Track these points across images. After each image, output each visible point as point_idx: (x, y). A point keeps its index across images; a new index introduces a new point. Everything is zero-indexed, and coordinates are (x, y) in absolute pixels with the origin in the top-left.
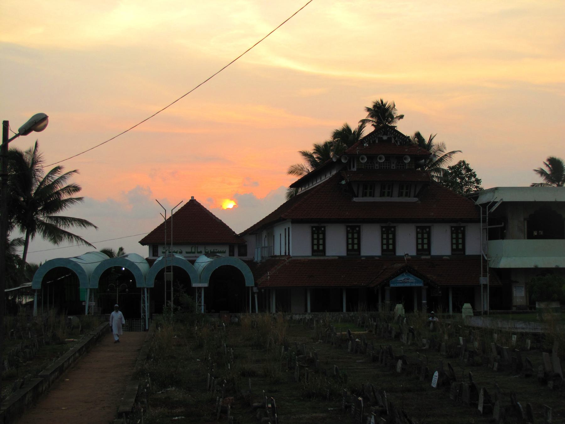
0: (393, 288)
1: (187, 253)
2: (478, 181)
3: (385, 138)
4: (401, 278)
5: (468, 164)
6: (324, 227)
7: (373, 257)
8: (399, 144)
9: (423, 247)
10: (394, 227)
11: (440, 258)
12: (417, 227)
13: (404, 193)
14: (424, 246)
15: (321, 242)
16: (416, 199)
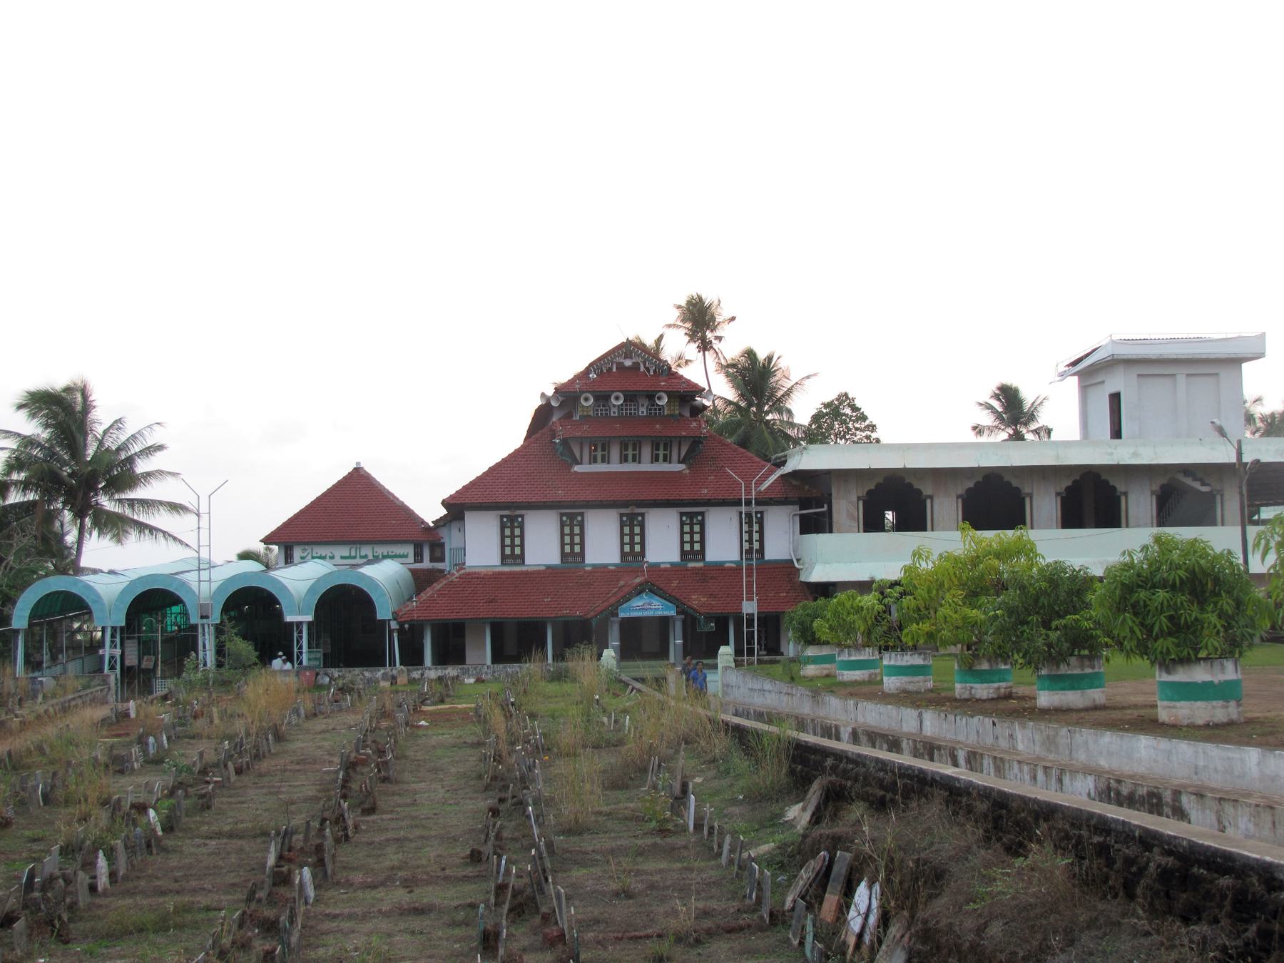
0: (623, 619)
1: (342, 558)
2: (872, 427)
3: (628, 363)
4: (637, 602)
6: (522, 516)
7: (605, 566)
9: (692, 547)
10: (643, 515)
11: (601, 569)
12: (682, 514)
13: (630, 458)
14: (693, 549)
15: (577, 539)
16: (682, 467)
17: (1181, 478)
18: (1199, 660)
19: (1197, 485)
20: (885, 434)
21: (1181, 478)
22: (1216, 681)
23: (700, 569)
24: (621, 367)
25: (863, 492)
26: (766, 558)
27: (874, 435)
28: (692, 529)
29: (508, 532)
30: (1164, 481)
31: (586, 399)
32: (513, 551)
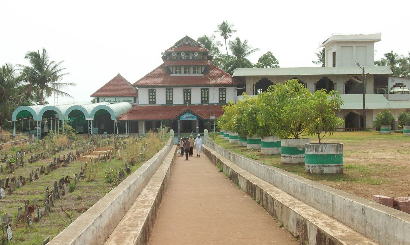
3: (187, 43)
4: (185, 116)
5: (272, 54)
8: (194, 46)
9: (205, 99)
10: (190, 89)
13: (187, 72)
17: (353, 79)
18: (269, 135)
19: (358, 81)
20: (281, 65)
21: (353, 79)
22: (275, 142)
23: (206, 106)
24: (185, 44)
25: (255, 83)
26: (191, 103)
27: (278, 65)
28: (205, 93)
29: (151, 94)
30: (348, 80)
31: (174, 54)
32: (170, 99)
